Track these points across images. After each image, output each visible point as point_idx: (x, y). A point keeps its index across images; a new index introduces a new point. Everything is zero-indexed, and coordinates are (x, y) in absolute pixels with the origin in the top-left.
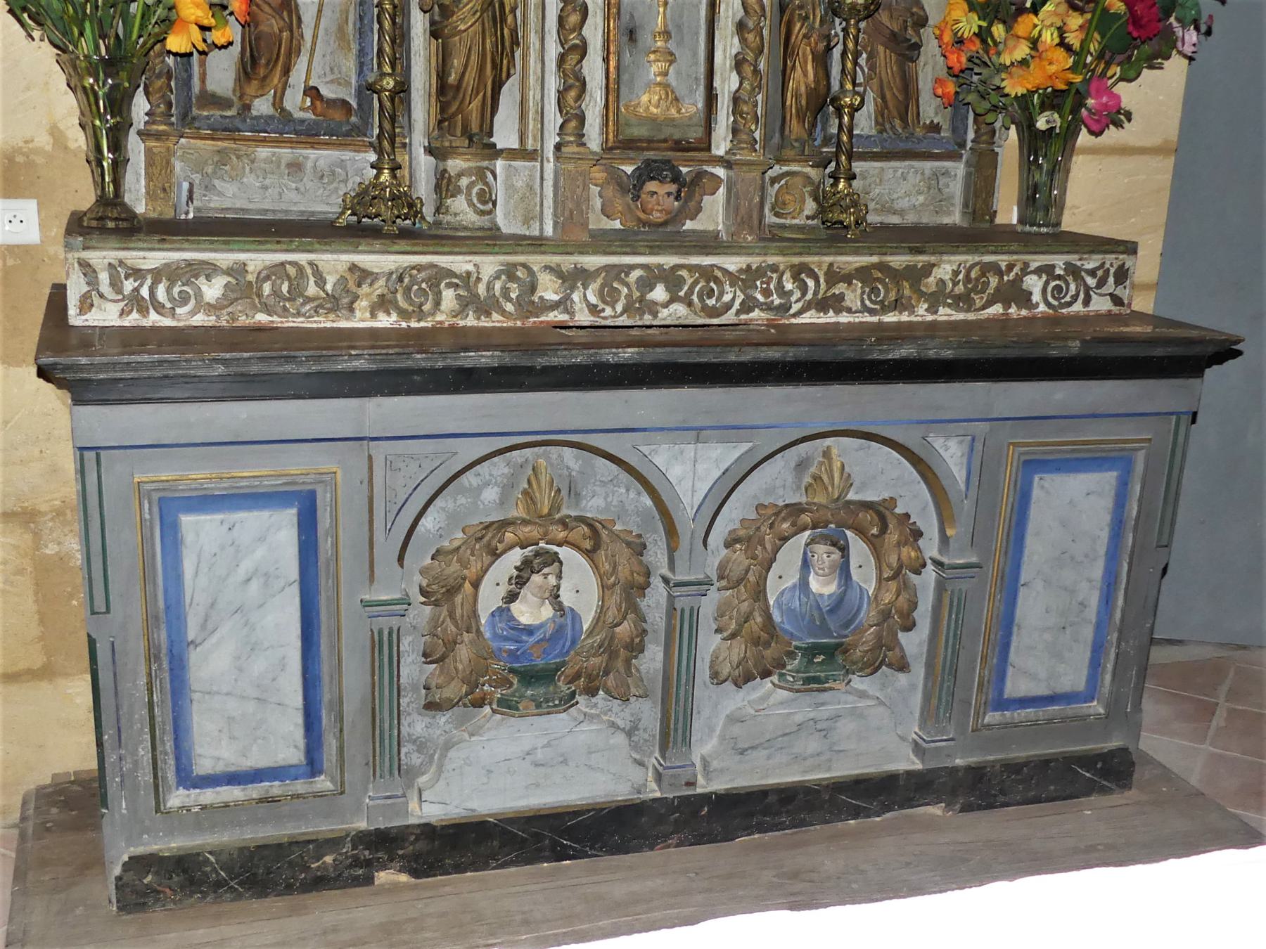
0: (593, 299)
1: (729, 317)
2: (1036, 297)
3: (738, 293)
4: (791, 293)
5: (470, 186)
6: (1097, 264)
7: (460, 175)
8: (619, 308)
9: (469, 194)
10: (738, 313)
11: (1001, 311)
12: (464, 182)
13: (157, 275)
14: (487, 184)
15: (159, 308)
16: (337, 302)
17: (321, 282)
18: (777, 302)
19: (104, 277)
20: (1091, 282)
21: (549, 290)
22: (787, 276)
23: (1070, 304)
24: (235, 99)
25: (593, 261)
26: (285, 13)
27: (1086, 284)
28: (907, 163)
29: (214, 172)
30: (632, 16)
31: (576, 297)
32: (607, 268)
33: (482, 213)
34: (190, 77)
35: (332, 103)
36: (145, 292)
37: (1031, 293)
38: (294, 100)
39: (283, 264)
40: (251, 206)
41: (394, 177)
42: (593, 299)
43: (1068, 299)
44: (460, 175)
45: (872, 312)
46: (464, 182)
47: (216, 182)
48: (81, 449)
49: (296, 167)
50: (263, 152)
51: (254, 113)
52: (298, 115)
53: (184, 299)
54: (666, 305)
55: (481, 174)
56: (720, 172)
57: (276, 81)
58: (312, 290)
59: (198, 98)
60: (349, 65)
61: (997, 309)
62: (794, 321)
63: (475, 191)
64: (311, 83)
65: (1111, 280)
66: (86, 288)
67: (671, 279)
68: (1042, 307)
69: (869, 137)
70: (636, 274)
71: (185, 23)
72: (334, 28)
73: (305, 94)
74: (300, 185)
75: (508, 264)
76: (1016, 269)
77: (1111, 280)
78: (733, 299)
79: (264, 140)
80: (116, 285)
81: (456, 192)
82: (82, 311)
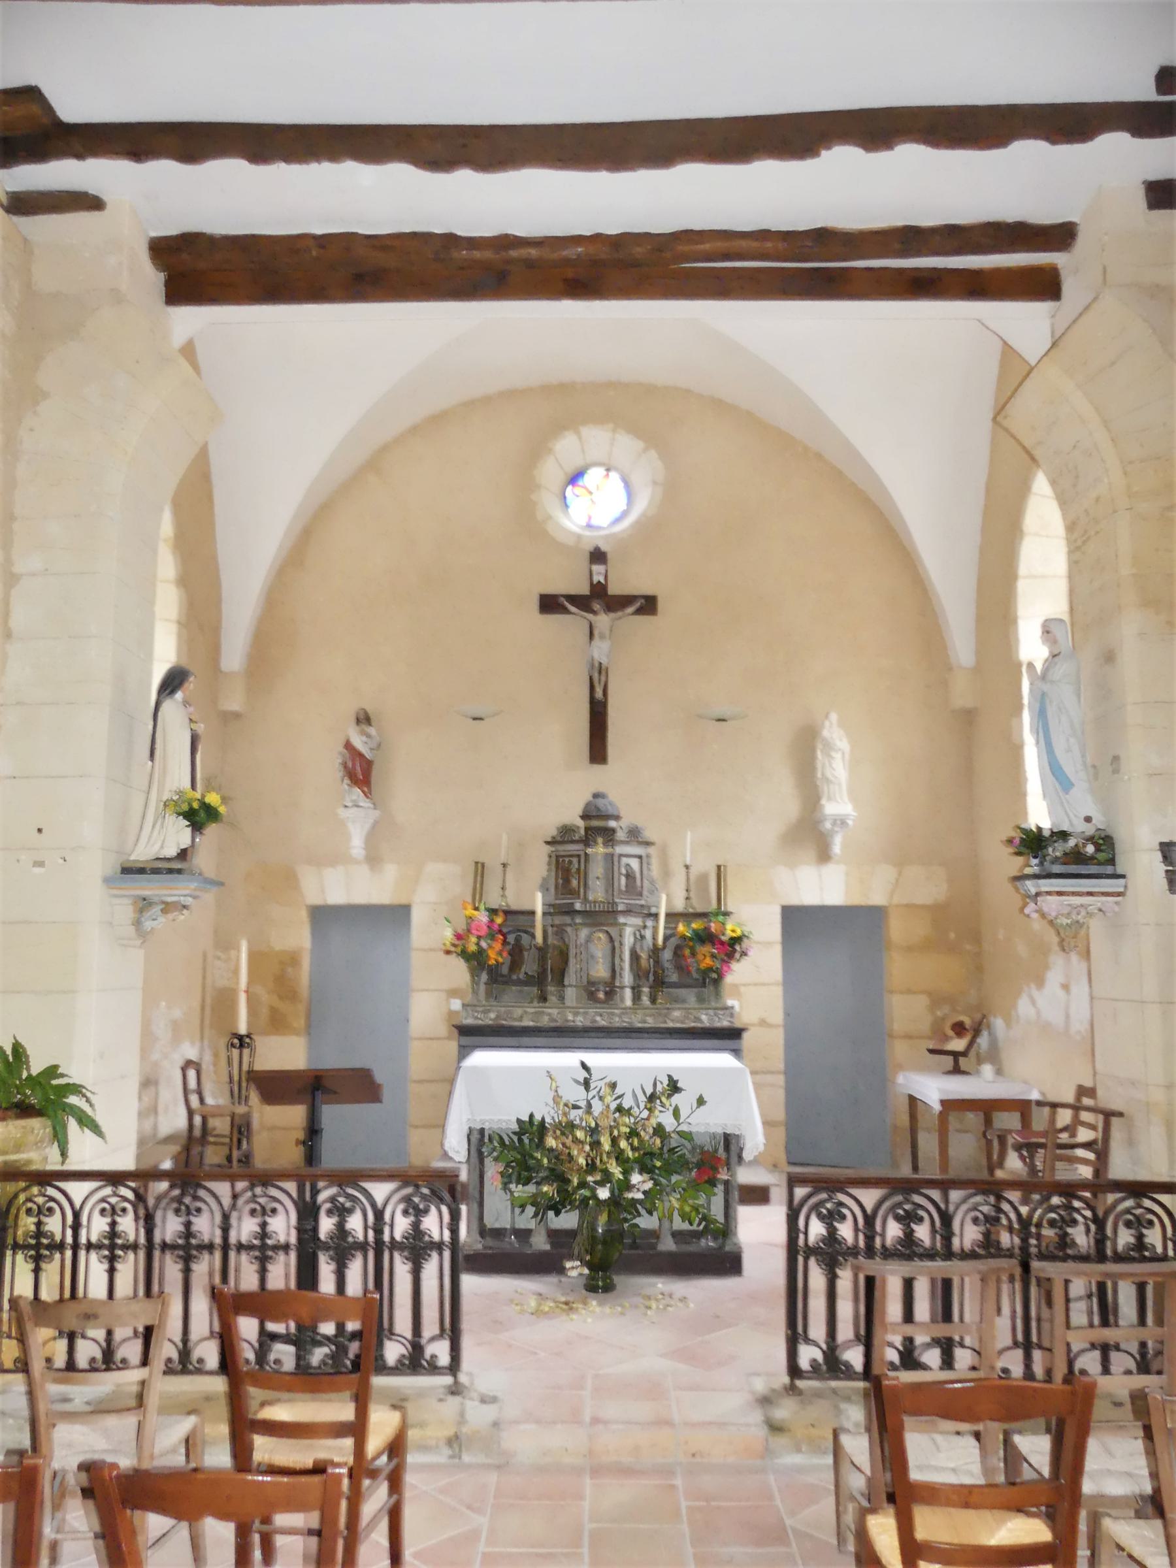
38: (522, 976)
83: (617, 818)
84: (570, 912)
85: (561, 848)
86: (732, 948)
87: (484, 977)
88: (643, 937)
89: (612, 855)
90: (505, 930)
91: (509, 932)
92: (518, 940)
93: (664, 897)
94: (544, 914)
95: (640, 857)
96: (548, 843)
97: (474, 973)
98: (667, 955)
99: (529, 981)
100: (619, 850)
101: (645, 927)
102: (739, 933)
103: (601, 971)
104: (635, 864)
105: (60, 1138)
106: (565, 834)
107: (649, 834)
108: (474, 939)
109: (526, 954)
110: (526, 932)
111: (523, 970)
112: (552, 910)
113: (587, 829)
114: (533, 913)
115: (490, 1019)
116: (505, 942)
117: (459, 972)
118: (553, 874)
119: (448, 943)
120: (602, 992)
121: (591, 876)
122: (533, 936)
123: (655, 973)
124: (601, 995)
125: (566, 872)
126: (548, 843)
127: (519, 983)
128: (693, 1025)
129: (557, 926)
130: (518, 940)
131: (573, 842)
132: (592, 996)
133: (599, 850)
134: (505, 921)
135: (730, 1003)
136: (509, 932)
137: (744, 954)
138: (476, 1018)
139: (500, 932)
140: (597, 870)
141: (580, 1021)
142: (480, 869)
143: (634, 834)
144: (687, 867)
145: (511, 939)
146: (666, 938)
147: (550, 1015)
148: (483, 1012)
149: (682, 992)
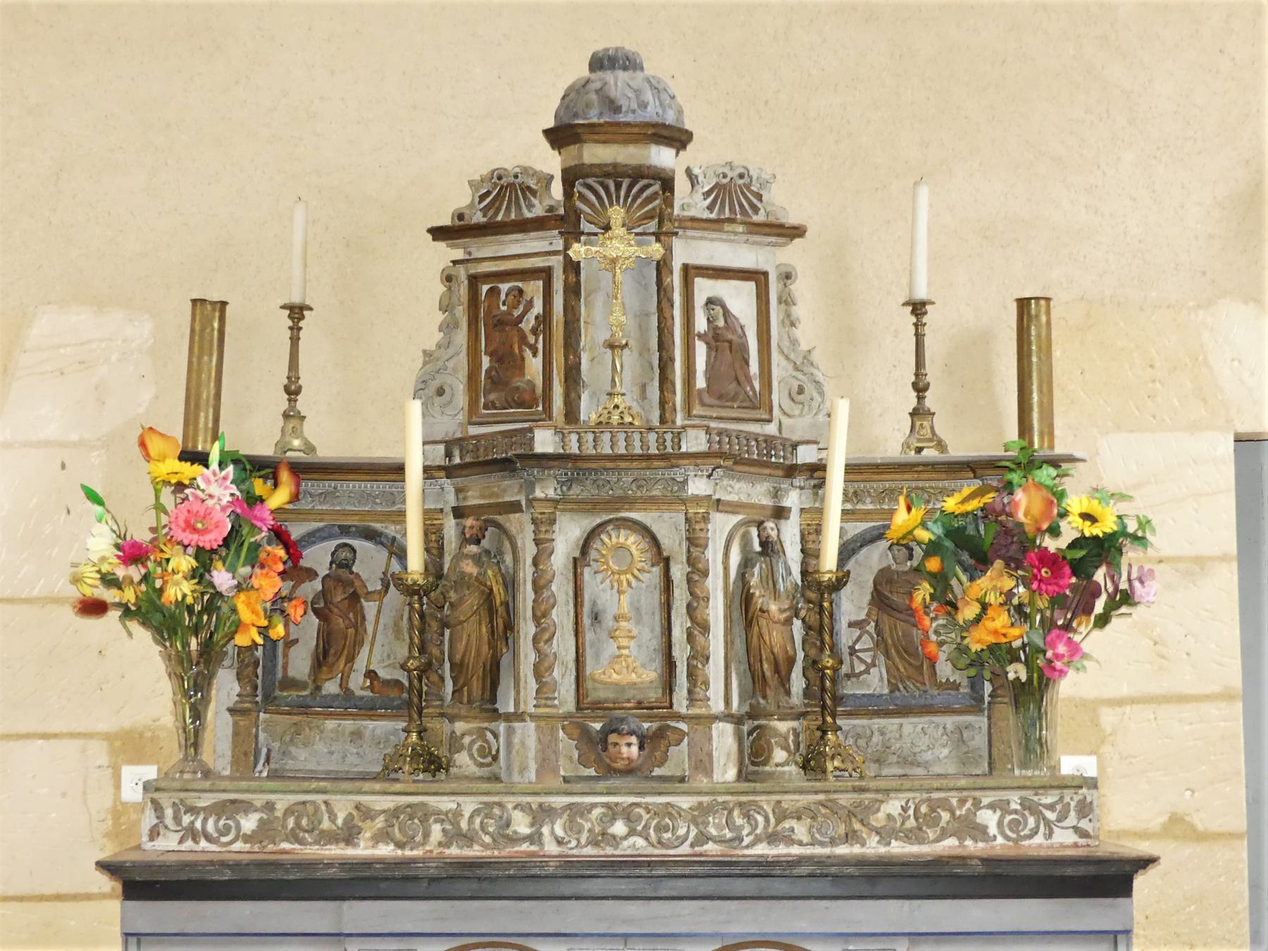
0: (559, 832)
1: (685, 849)
2: (993, 830)
3: (692, 827)
4: (742, 827)
5: (473, 742)
6: (1056, 799)
7: (463, 735)
8: (583, 841)
9: (470, 749)
10: (692, 845)
11: (957, 843)
12: (467, 740)
13: (209, 811)
14: (486, 741)
15: (209, 838)
16: (349, 835)
17: (333, 818)
18: (729, 835)
19: (169, 812)
20: (1051, 816)
21: (521, 825)
22: (736, 813)
23: (1030, 837)
24: (310, 682)
25: (559, 801)
26: (351, 615)
27: (1044, 818)
28: (927, 719)
29: (292, 740)
30: (594, 603)
31: (545, 830)
32: (570, 806)
33: (481, 765)
34: (275, 666)
35: (387, 683)
36: (198, 825)
37: (987, 827)
38: (357, 682)
39: (304, 803)
40: (320, 768)
41: (421, 739)
42: (559, 832)
43: (1026, 832)
44: (463, 735)
45: (822, 844)
46: (467, 740)
47: (292, 749)
48: (127, 935)
49: (357, 735)
50: (330, 724)
51: (324, 692)
52: (359, 693)
53: (227, 830)
54: (625, 838)
55: (481, 733)
56: (683, 726)
57: (342, 666)
58: (326, 824)
59: (280, 683)
60: (402, 651)
61: (951, 842)
62: (747, 852)
63: (476, 746)
64: (372, 668)
65: (1073, 814)
66: (155, 821)
67: (628, 815)
68: (1000, 840)
69: (881, 696)
70: (597, 812)
71: (246, 626)
72: (391, 623)
73: (365, 676)
74: (361, 750)
75: (485, 803)
76: (968, 805)
77: (1073, 814)
78: (688, 832)
79: (331, 714)
80: (177, 820)
81: (461, 748)
82: (152, 839)
83: (678, 138)
84: (516, 461)
85: (486, 248)
86: (1085, 575)
87: (226, 687)
88: (769, 548)
89: (662, 267)
90: (296, 531)
91: (312, 538)
92: (343, 562)
93: (842, 410)
94: (428, 471)
95: (757, 277)
96: (438, 233)
97: (194, 683)
98: (852, 605)
99: (385, 699)
100: (686, 251)
101: (780, 513)
102: (1107, 525)
103: (627, 664)
104: (740, 300)
105: (368, 839)
106: (499, 207)
107: (783, 201)
108: (184, 563)
109: (370, 608)
110: (371, 535)
111: (361, 663)
112: (458, 462)
113: (570, 176)
114: (397, 470)
115: (235, 841)
116: (295, 571)
117: (137, 672)
118: (461, 337)
119: (91, 575)
120: (619, 738)
121: (592, 335)
122: (400, 553)
123: (813, 665)
124: (630, 750)
125: (504, 332)
126: (438, 233)
127: (348, 704)
128: (949, 845)
129: (476, 510)
130: (343, 562)
131: (524, 226)
132: (596, 747)
133: (615, 249)
134: (295, 498)
135: (1070, 764)
136: (312, 538)
137: (1124, 598)
138: (192, 833)
139: (279, 535)
140: (613, 313)
141: (553, 842)
142: (209, 318)
143: (736, 203)
144: (918, 308)
145: (318, 557)
146: (847, 551)
147: (452, 819)
148: (219, 810)
149: (910, 731)
